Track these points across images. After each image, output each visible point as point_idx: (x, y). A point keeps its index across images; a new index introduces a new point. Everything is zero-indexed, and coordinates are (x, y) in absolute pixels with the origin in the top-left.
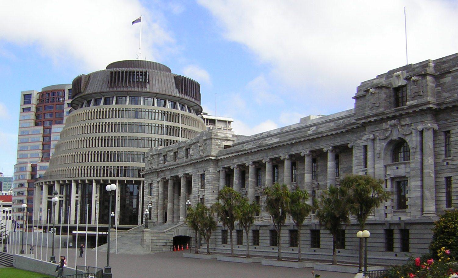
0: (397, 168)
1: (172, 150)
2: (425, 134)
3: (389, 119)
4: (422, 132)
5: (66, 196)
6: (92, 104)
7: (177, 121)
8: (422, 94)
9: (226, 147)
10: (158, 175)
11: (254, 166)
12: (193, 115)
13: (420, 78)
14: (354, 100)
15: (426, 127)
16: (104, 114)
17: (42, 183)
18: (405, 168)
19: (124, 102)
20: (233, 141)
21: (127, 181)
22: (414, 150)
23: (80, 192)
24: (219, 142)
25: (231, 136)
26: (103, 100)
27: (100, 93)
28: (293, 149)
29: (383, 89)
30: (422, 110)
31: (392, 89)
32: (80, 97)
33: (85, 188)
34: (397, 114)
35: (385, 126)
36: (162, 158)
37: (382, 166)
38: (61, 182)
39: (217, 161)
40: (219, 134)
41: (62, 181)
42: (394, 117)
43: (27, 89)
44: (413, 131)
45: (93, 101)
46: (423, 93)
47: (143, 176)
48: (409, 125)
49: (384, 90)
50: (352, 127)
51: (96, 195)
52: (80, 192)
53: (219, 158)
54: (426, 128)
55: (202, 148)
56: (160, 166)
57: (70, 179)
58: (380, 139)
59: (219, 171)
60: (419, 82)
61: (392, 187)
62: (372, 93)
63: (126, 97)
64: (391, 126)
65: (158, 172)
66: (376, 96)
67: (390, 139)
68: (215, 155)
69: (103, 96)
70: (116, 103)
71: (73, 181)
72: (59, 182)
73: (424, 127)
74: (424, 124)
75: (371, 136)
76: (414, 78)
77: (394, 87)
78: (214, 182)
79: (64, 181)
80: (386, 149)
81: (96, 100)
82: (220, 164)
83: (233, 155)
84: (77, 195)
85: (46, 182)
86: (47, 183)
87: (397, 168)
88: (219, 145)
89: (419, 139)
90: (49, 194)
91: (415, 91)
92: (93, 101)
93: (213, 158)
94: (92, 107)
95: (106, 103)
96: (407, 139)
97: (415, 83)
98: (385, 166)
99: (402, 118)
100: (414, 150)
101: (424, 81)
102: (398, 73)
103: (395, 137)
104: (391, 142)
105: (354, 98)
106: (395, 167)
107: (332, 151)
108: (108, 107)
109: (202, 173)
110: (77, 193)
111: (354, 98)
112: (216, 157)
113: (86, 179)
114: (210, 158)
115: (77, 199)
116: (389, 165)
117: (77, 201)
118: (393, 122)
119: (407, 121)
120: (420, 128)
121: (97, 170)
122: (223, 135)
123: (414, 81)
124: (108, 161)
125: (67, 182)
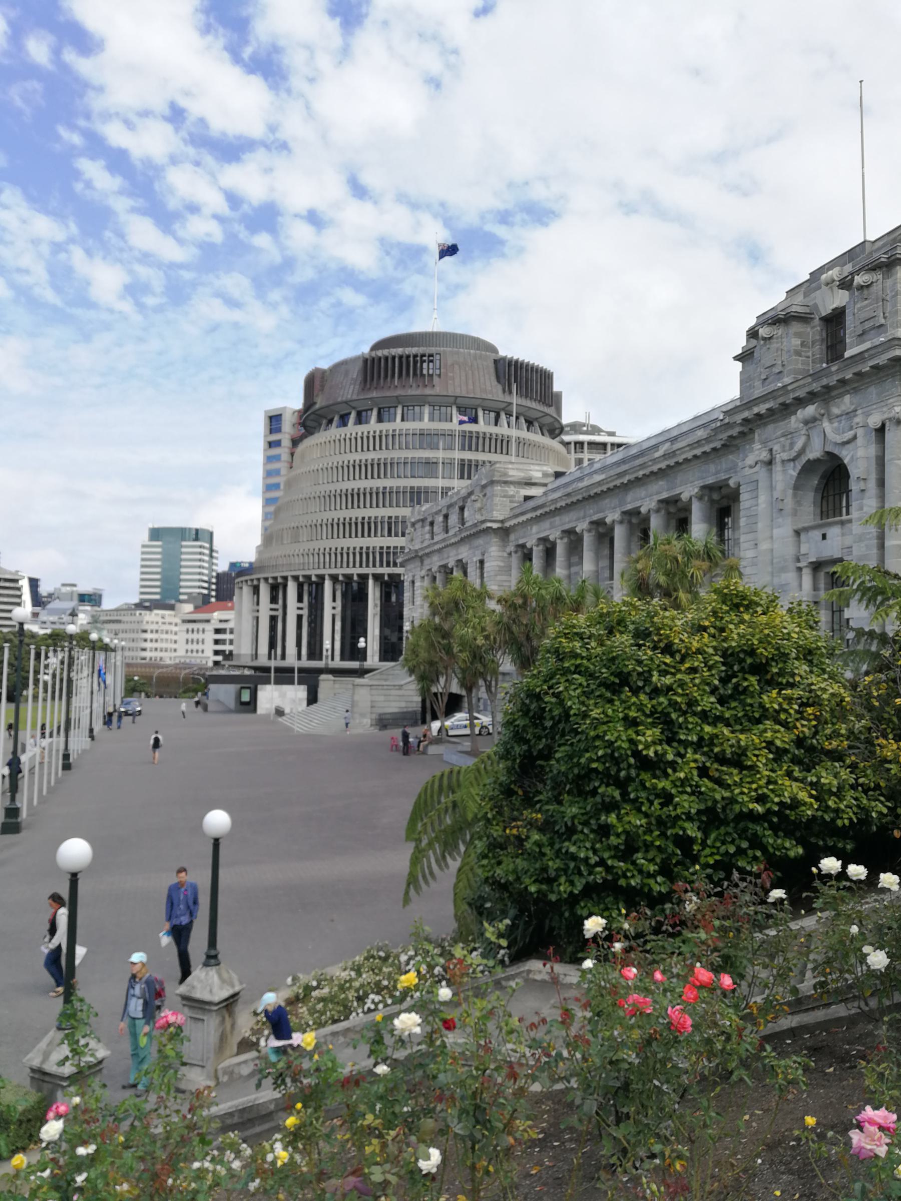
0: (824, 537)
1: (440, 511)
2: (888, 436)
3: (800, 402)
4: (881, 431)
5: (310, 605)
6: (335, 423)
7: (504, 451)
8: (882, 321)
9: (527, 498)
10: (422, 562)
11: (566, 540)
12: (546, 440)
13: (878, 276)
14: (739, 365)
15: (891, 415)
16: (378, 441)
17: (259, 580)
18: (843, 535)
19: (392, 416)
20: (545, 485)
21: (389, 575)
22: (862, 485)
23: (306, 598)
24: (511, 490)
25: (539, 475)
26: (375, 412)
27: (346, 402)
28: (629, 497)
29: (794, 323)
30: (875, 367)
31: (817, 321)
32: (313, 413)
33: (311, 589)
34: (816, 387)
35: (794, 422)
36: (427, 528)
37: (791, 533)
38: (301, 579)
39: (504, 532)
40: (511, 473)
41: (304, 576)
42: (812, 397)
43: (275, 404)
44: (860, 432)
45: (336, 419)
46: (885, 318)
47: (402, 566)
48: (850, 415)
49: (796, 327)
50: (730, 433)
51: (334, 604)
52: (306, 598)
53: (507, 524)
54: (890, 419)
55: (478, 505)
56: (426, 543)
57: (284, 574)
58: (783, 461)
59: (510, 554)
60: (874, 288)
61: (815, 588)
62: (765, 339)
63: (396, 407)
64: (806, 422)
65: (421, 557)
66: (774, 345)
67: (804, 459)
68: (501, 518)
69: (354, 408)
70: (403, 420)
71: (327, 577)
72: (296, 578)
73: (886, 416)
74: (885, 409)
75: (764, 455)
76: (858, 280)
77: (824, 314)
78: (499, 578)
79: (308, 577)
80: (797, 487)
81: (359, 414)
82: (512, 537)
83: (529, 516)
84: (300, 605)
85: (266, 579)
86: (271, 581)
87: (824, 537)
88: (513, 496)
89: (872, 450)
90: (272, 602)
91: (864, 315)
92: (336, 419)
93: (495, 526)
94: (352, 429)
95: (380, 420)
96: (846, 455)
97: (865, 292)
98: (797, 533)
99: (834, 398)
100: (862, 485)
101: (889, 282)
102: (830, 272)
103: (815, 452)
104: (809, 467)
105: (737, 358)
106: (817, 534)
107: (700, 498)
108: (386, 426)
109: (480, 558)
110: (300, 599)
111: (737, 358)
112: (502, 522)
113: (313, 573)
114: (489, 525)
115: (300, 612)
116: (806, 529)
117: (334, 616)
118: (811, 410)
119: (847, 402)
120: (875, 420)
121: (342, 555)
122: (522, 475)
123: (861, 288)
124: (363, 536)
125: (280, 580)
